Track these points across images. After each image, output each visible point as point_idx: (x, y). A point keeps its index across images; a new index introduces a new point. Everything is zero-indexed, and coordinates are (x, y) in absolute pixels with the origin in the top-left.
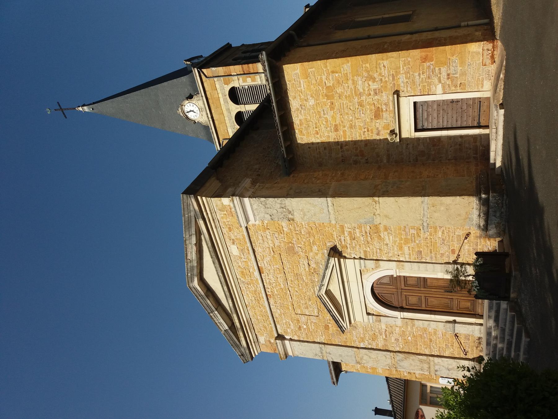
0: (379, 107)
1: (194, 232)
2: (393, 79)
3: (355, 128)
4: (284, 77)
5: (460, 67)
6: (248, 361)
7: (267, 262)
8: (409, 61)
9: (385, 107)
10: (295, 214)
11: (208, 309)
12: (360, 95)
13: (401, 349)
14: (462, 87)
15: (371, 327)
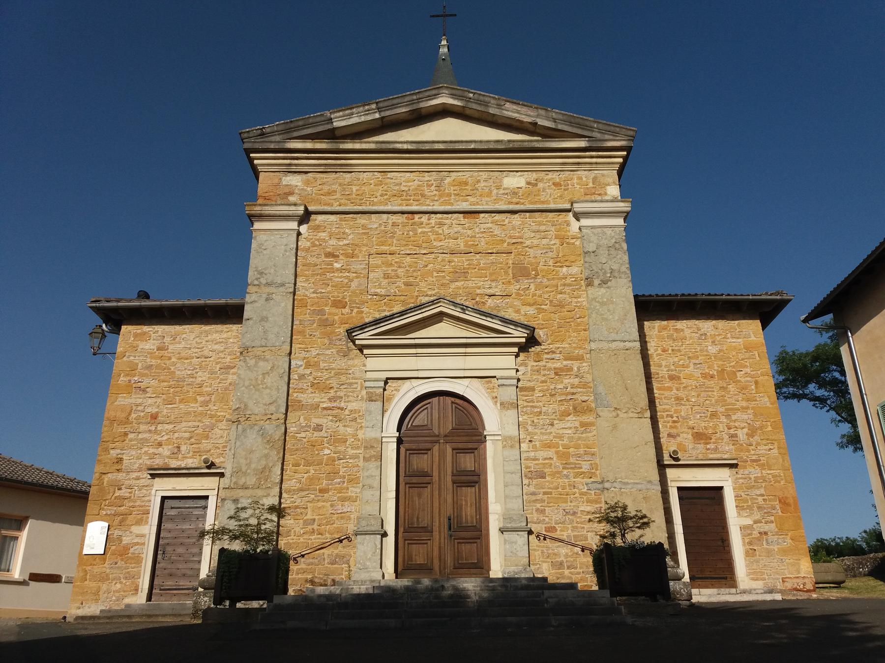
0: (711, 439)
1: (560, 127)
2: (753, 461)
3: (677, 404)
4: (744, 319)
5: (778, 549)
6: (244, 140)
7: (491, 228)
8: (780, 482)
9: (713, 447)
10: (603, 290)
11: (386, 104)
12: (728, 416)
13: (292, 434)
14: (751, 551)
15: (351, 384)
